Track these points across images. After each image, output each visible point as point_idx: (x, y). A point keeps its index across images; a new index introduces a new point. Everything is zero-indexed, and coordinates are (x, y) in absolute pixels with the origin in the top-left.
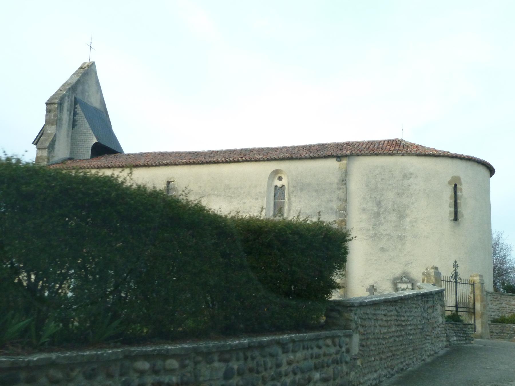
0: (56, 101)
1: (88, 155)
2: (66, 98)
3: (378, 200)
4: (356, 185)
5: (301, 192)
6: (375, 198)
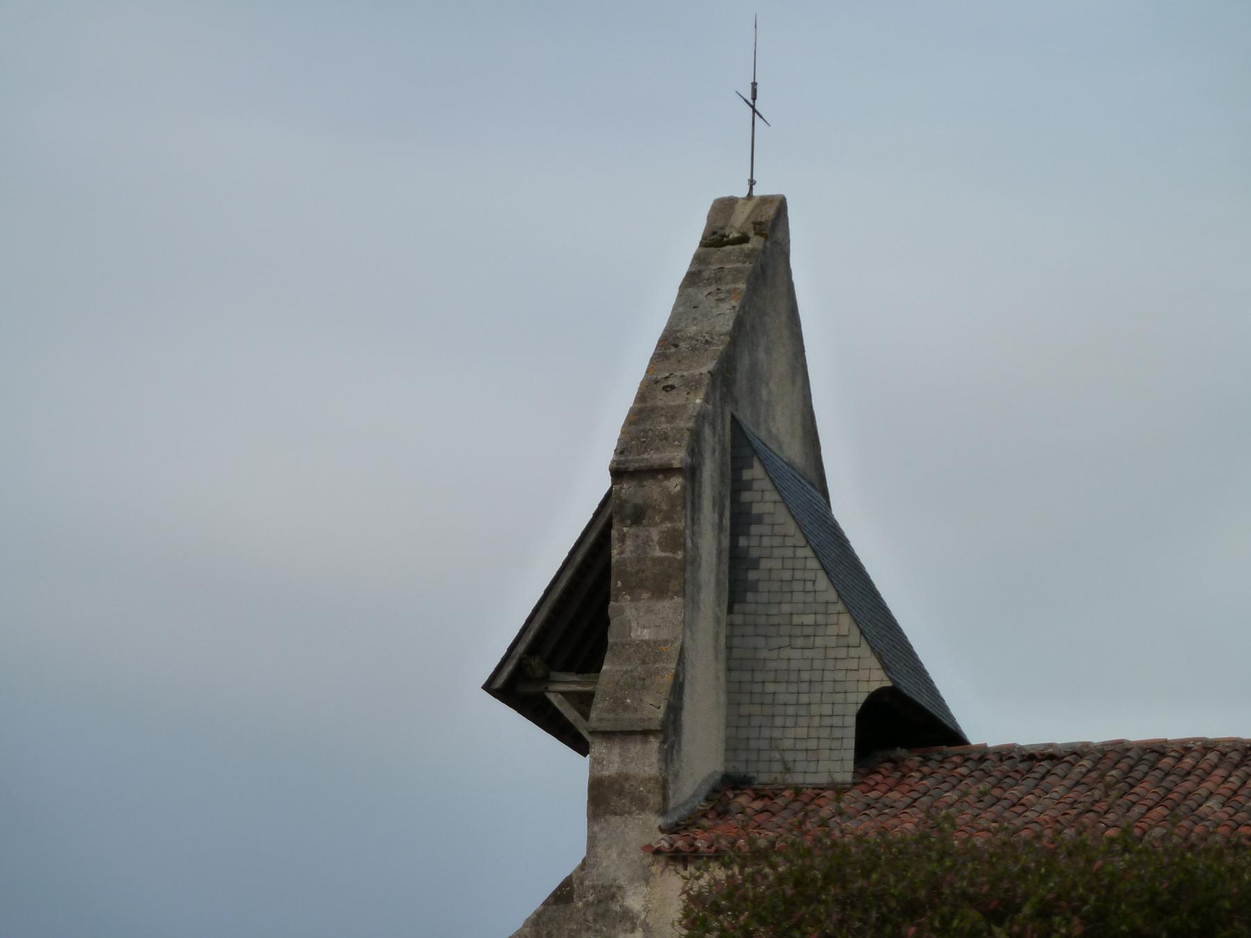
1: (838, 762)
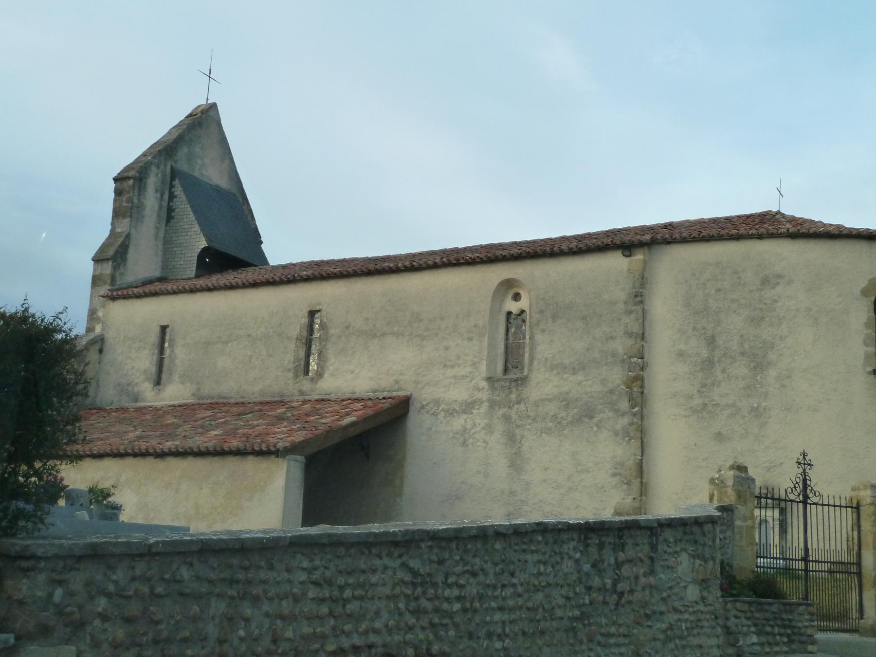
0: (131, 173)
2: (153, 168)
3: (709, 333)
4: (664, 304)
5: (554, 321)
6: (704, 328)
